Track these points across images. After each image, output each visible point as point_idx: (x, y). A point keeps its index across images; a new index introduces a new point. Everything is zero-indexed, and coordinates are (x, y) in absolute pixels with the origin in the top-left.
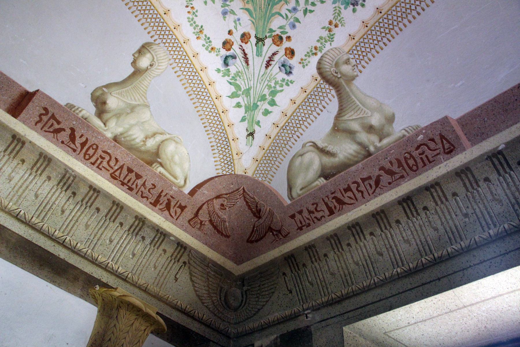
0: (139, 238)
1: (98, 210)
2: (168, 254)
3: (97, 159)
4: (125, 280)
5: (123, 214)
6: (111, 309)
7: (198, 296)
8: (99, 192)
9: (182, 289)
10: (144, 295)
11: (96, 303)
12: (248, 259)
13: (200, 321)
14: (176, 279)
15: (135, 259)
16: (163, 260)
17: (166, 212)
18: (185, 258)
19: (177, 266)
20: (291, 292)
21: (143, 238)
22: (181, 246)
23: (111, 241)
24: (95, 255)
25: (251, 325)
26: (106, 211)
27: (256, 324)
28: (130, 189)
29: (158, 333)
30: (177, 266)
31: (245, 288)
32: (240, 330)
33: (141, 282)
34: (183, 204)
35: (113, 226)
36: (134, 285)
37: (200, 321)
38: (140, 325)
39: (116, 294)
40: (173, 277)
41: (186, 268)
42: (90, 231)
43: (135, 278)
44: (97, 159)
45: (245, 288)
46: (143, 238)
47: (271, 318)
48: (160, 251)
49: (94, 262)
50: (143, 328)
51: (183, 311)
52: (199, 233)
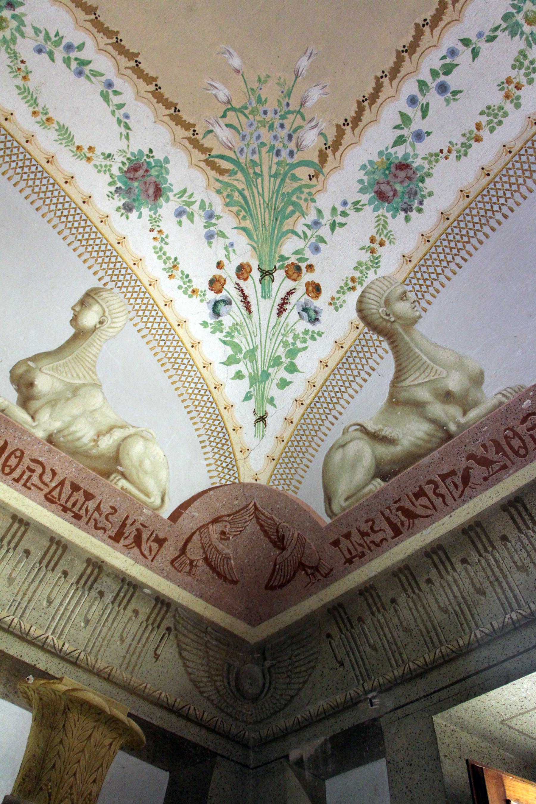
0: (94, 593)
1: (27, 553)
2: (142, 617)
3: (23, 473)
4: (75, 663)
5: (68, 557)
6: (52, 714)
7: (193, 681)
8: (27, 524)
9: (167, 672)
10: (107, 686)
11: (28, 705)
12: (270, 617)
13: (199, 723)
14: (157, 657)
15: (90, 628)
16: (134, 627)
17: (136, 550)
18: (168, 622)
19: (156, 636)
20: (342, 664)
21: (101, 594)
22: (162, 602)
23: (50, 602)
24: (26, 626)
25: (282, 722)
26: (40, 554)
27: (290, 722)
28: (77, 517)
29: (132, 748)
30: (156, 636)
31: (267, 664)
32: (264, 733)
33: (101, 665)
34: (161, 536)
35: (53, 577)
36: (91, 671)
37: (199, 723)
38: (102, 736)
39: (62, 687)
40: (151, 653)
41: (172, 637)
42: (15, 588)
43: (91, 659)
44: (23, 473)
45: (267, 664)
46: (101, 594)
47: (313, 709)
48: (129, 612)
49: (24, 637)
50: (107, 741)
51: (170, 709)
52: (188, 579)
